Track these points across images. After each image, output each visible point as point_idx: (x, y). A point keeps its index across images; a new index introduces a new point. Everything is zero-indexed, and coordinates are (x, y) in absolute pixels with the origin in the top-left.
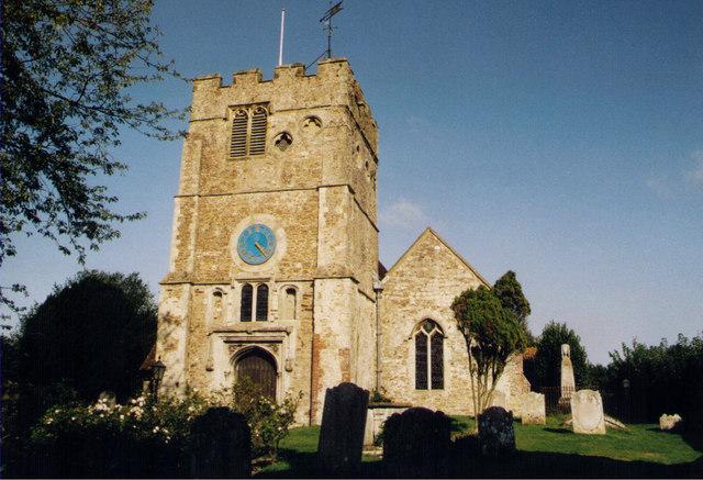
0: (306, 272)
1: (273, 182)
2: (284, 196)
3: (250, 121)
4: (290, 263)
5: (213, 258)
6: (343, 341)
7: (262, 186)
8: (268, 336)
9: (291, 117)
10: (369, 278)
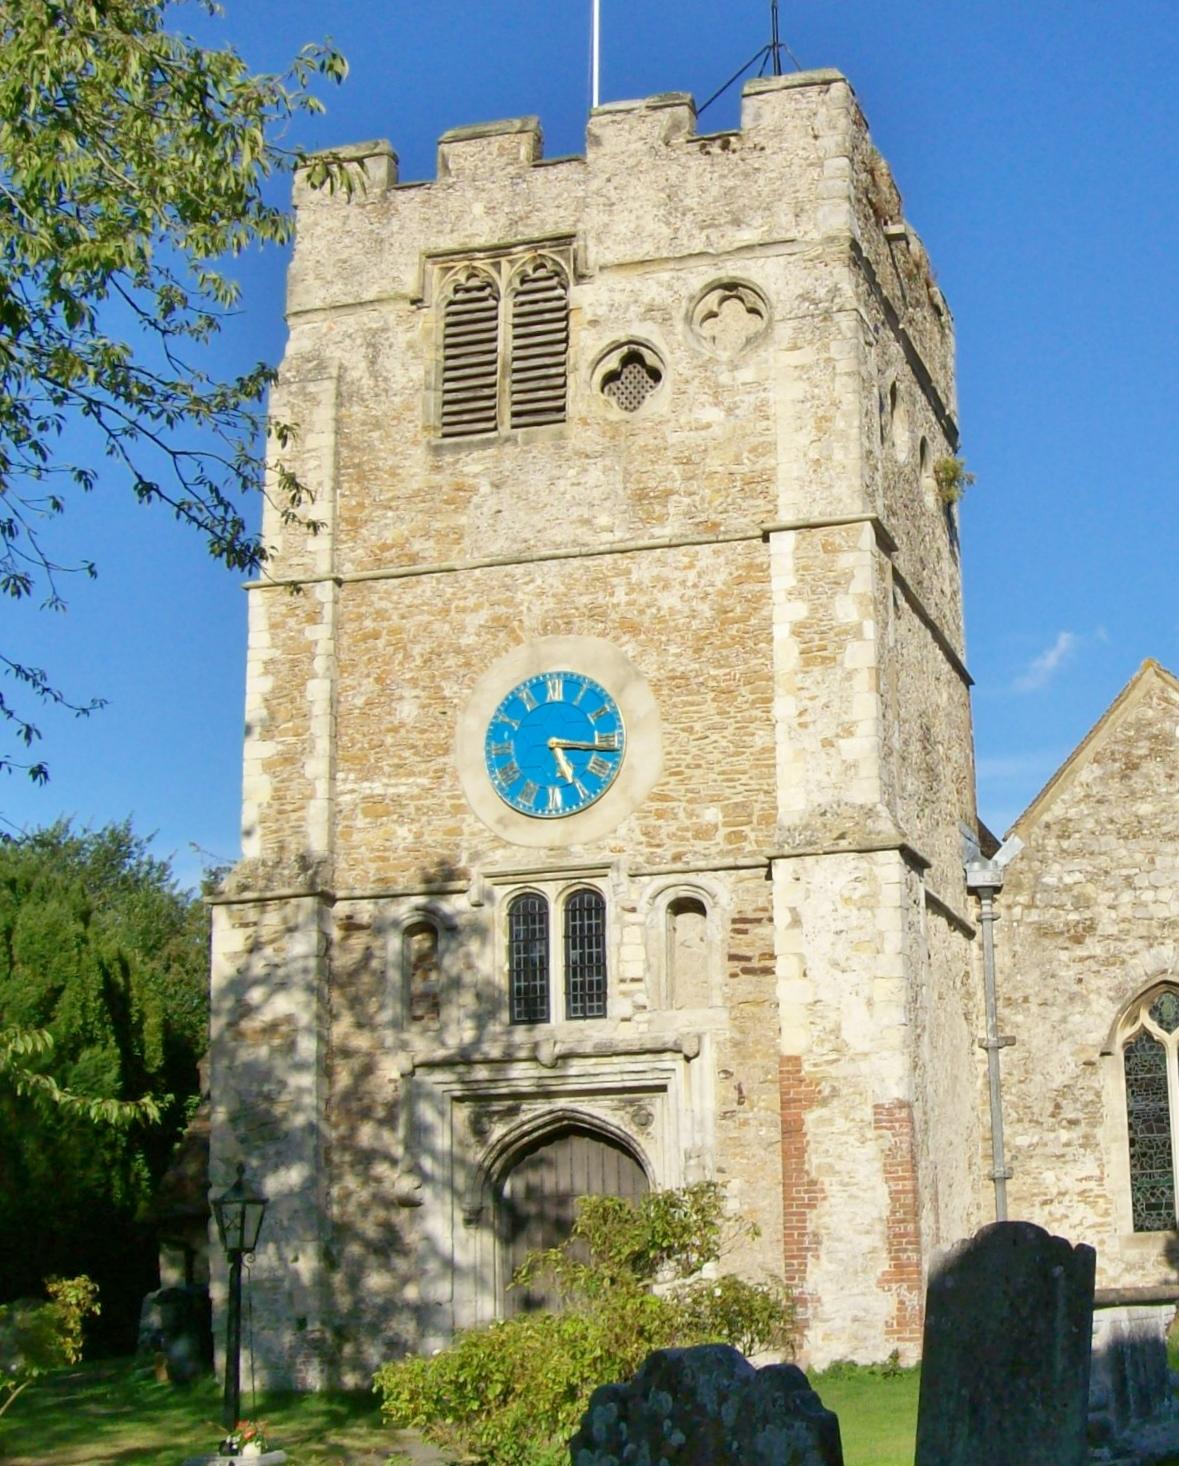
0: (740, 837)
1: (603, 520)
2: (643, 569)
3: (506, 308)
4: (680, 807)
5: (397, 800)
6: (891, 1080)
7: (563, 535)
8: (613, 1072)
9: (654, 287)
10: (946, 847)
